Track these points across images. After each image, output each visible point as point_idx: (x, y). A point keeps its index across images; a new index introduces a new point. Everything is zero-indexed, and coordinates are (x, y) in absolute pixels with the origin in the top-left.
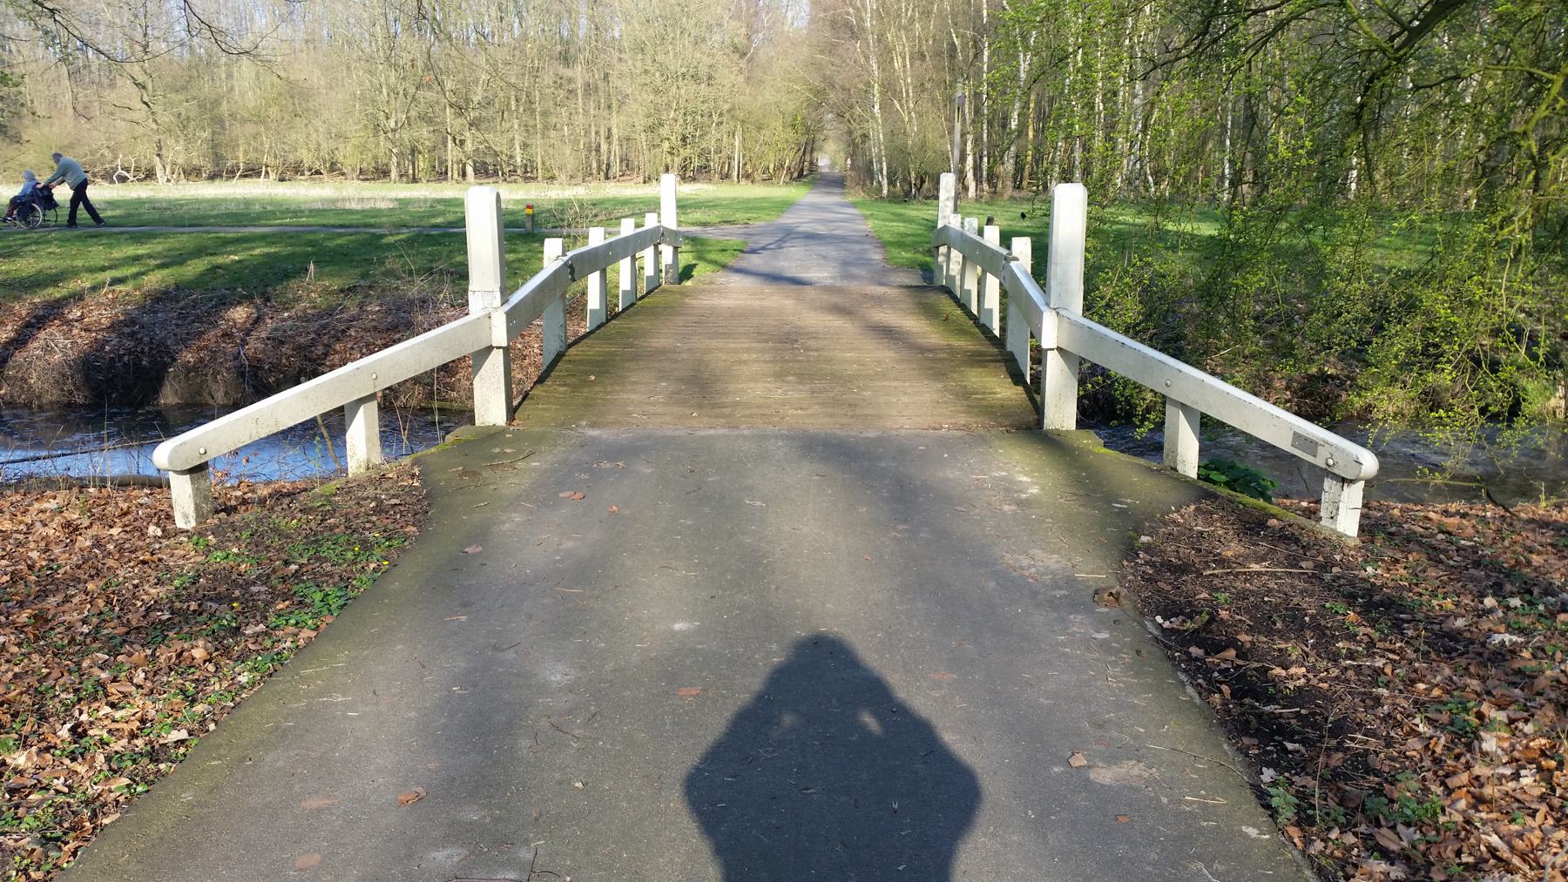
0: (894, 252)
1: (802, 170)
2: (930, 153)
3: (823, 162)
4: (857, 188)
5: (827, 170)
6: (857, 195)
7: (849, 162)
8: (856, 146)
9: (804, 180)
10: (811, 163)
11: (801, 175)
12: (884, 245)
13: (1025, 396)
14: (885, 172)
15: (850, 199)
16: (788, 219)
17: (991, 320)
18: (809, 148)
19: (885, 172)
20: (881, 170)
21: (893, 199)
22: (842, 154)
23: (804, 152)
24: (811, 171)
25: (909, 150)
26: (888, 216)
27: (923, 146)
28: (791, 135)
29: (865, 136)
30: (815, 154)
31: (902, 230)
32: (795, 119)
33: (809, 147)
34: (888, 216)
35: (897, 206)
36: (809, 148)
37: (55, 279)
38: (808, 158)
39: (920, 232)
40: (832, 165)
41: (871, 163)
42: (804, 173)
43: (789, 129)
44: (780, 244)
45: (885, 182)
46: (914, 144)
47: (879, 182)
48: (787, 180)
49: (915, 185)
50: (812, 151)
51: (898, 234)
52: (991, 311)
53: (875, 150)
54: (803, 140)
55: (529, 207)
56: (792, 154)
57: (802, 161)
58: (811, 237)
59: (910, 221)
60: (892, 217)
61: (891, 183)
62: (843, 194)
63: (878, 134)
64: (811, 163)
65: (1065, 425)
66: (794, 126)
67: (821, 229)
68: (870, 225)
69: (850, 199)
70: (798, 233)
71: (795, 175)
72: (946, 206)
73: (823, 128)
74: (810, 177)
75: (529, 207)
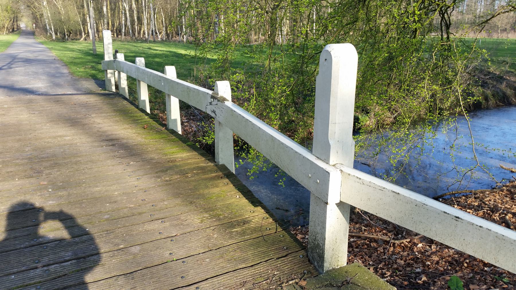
0: (74, 68)
1: (14, 29)
2: (72, 22)
3: (22, 25)
4: (42, 36)
5: (24, 29)
6: (42, 39)
7: (34, 25)
8: (37, 19)
9: (15, 32)
10: (17, 26)
11: (13, 31)
12: (66, 65)
13: (271, 220)
14: (53, 30)
15: (39, 41)
16: (12, 51)
17: (176, 125)
18: (15, 20)
19: (53, 30)
20: (51, 29)
21: (57, 40)
22: (30, 22)
23: (13, 22)
24: (18, 29)
25: (63, 20)
26: (59, 48)
27: (69, 20)
28: (6, 14)
29: (42, 15)
30: (18, 22)
31: (71, 55)
32: (7, 8)
33: (16, 19)
34: (59, 48)
35: (62, 43)
36: (15, 20)
37: (152, 31)
38: (15, 24)
39: (80, 56)
40: (27, 27)
41: (45, 25)
42: (14, 30)
43: (5, 12)
44: (10, 65)
45: (53, 34)
46: (65, 18)
47: (50, 33)
48: (7, 32)
49: (67, 34)
50: (17, 21)
51: (72, 57)
52: (175, 120)
53: (47, 21)
54: (12, 16)
55: (64, 41)
56: (8, 22)
57: (13, 25)
58: (28, 61)
59: (73, 50)
60: (62, 49)
61: (56, 34)
62: (35, 38)
63: (47, 13)
64: (17, 26)
65: (340, 263)
66: (7, 11)
67: (31, 56)
68: (54, 54)
69: (39, 41)
70: (18, 59)
71: (11, 30)
72: (109, 47)
73: (20, 12)
74: (18, 31)
75: (64, 41)
